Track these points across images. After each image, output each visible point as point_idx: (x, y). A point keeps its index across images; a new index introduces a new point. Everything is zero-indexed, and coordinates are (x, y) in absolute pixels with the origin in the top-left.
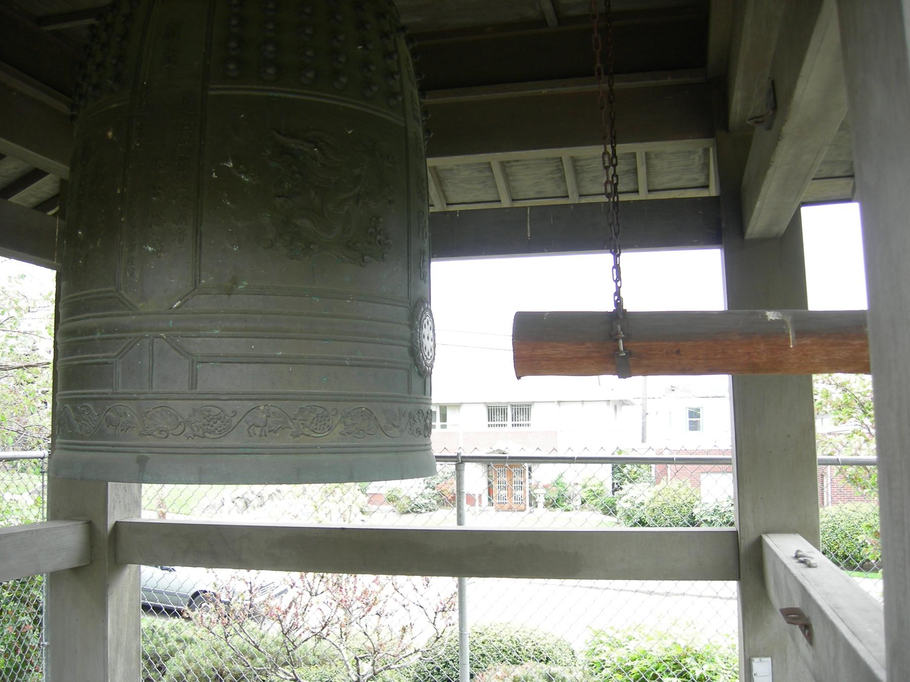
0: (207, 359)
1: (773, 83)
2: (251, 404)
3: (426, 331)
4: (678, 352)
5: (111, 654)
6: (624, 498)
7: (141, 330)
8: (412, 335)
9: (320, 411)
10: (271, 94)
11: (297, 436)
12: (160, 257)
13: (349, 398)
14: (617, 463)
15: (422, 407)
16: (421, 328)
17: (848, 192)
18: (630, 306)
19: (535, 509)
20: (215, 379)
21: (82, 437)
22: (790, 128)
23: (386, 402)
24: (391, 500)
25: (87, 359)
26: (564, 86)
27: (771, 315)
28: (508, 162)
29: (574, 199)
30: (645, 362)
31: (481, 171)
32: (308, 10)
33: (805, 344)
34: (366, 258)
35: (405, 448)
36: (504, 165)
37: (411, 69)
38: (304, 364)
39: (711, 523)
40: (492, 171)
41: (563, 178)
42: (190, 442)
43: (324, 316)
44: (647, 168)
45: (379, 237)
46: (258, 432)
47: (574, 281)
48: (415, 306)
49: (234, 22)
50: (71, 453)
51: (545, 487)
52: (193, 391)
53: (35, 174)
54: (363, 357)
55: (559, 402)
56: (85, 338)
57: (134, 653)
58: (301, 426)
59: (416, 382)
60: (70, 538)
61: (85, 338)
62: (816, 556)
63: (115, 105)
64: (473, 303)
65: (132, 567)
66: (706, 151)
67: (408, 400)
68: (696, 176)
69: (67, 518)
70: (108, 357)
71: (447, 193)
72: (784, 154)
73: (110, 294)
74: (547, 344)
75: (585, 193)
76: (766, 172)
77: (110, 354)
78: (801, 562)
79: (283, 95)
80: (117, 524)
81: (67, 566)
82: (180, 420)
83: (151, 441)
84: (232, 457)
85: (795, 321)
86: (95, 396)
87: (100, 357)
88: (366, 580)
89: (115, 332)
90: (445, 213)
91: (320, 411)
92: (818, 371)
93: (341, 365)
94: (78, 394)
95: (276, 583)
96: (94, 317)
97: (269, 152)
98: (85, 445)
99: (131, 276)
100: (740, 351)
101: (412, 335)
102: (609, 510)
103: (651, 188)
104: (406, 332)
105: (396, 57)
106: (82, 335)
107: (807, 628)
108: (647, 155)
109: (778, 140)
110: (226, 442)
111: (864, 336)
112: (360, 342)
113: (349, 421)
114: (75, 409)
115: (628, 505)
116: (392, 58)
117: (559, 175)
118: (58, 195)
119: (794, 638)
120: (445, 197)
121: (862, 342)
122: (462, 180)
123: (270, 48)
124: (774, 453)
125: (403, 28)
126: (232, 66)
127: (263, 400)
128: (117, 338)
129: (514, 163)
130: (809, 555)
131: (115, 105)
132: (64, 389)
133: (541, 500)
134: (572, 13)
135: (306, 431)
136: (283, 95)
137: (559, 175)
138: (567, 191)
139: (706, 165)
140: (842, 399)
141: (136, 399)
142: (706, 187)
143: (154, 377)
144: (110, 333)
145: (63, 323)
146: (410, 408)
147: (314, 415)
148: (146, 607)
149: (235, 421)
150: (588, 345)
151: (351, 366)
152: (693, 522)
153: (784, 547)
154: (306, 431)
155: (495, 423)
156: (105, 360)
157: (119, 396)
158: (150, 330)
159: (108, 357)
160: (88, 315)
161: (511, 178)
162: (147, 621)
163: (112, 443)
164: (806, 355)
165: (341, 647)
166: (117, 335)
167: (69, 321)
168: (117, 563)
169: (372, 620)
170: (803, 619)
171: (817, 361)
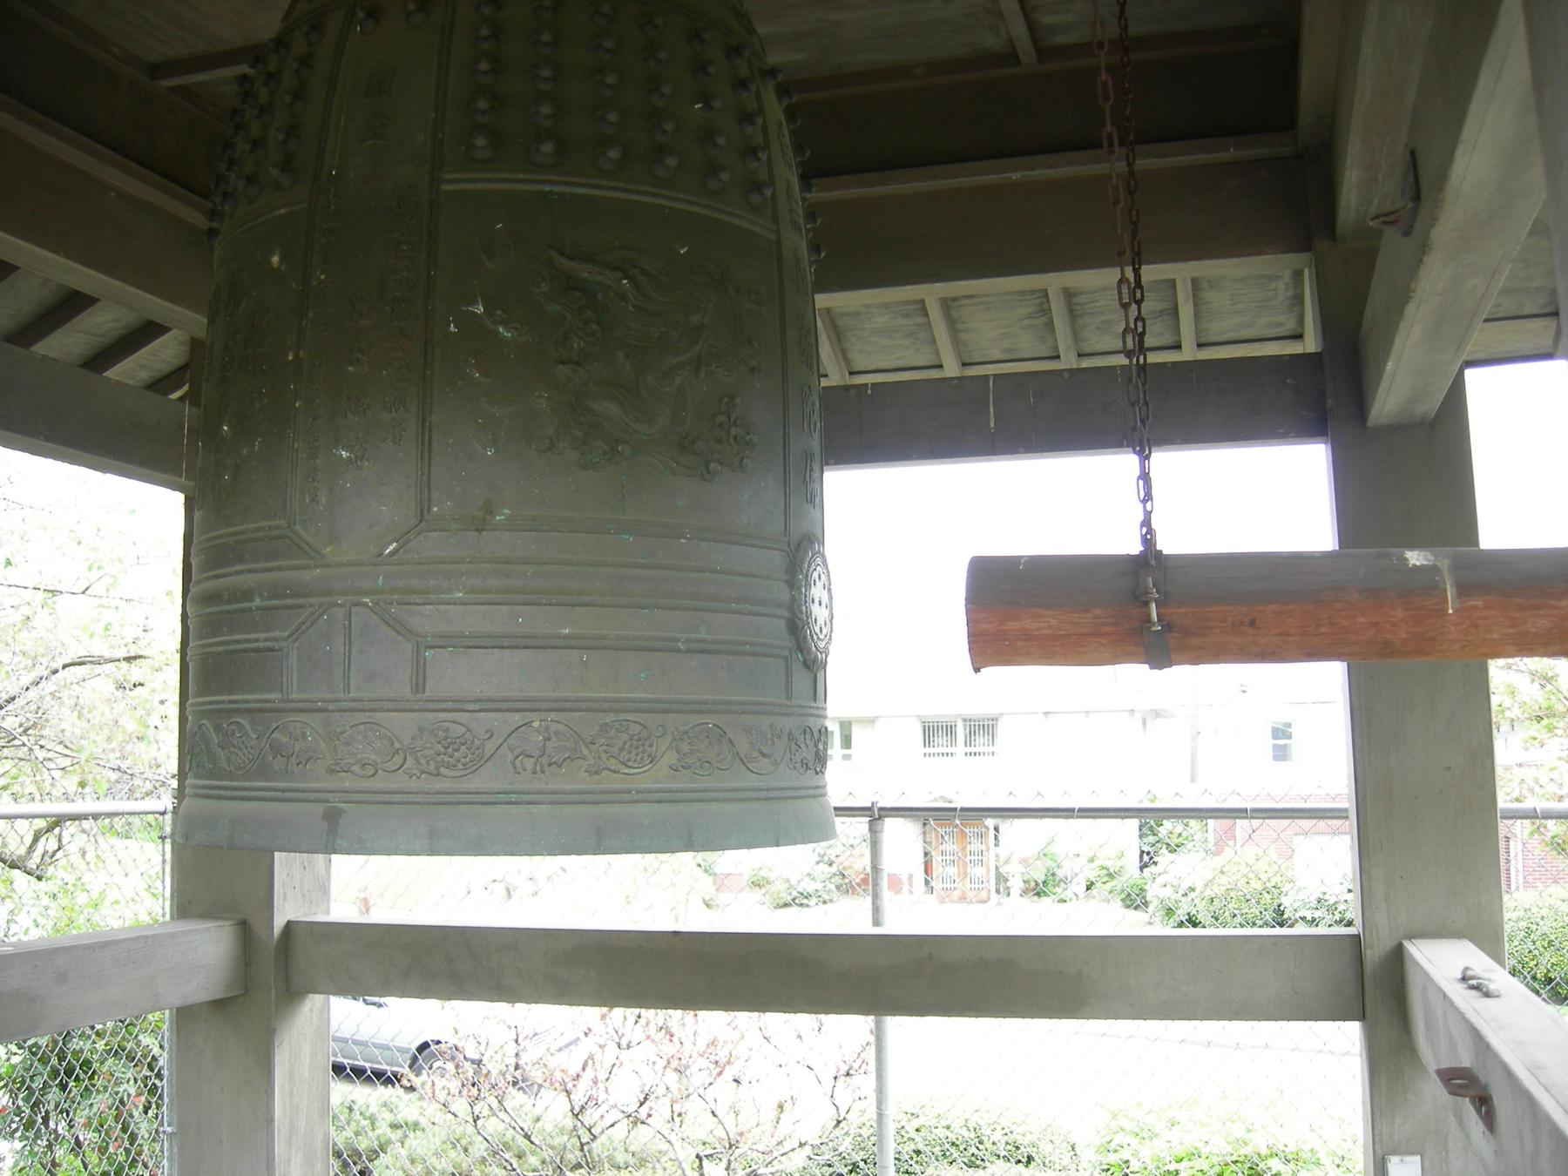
0: (445, 641)
1: (1413, 154)
2: (517, 719)
3: (817, 592)
4: (1252, 623)
5: (280, 1148)
6: (1160, 880)
7: (328, 593)
8: (793, 598)
9: (636, 729)
10: (547, 188)
11: (597, 773)
12: (361, 468)
14: (1149, 817)
15: (811, 721)
16: (808, 586)
17: (1546, 342)
18: (1169, 544)
19: (1007, 899)
20: (456, 675)
22: (1443, 232)
24: (756, 884)
25: (238, 642)
26: (1051, 166)
27: (1415, 558)
28: (955, 299)
29: (1068, 361)
30: (1196, 641)
31: (907, 316)
33: (1475, 608)
34: (712, 465)
36: (947, 304)
37: (787, 140)
38: (607, 648)
39: (1313, 922)
40: (927, 315)
41: (1050, 325)
42: (414, 784)
43: (641, 566)
44: (1196, 306)
45: (733, 431)
46: (530, 767)
47: (1073, 503)
51: (1024, 861)
52: (419, 696)
53: (148, 331)
54: (709, 637)
55: (1046, 713)
57: (319, 1146)
58: (604, 756)
59: (800, 678)
60: (209, 948)
62: (1498, 978)
63: (283, 211)
64: (899, 540)
65: (317, 999)
66: (1298, 274)
68: (1281, 318)
70: (274, 639)
72: (1434, 278)
73: (277, 532)
74: (1029, 610)
77: (277, 634)
78: (1473, 987)
79: (568, 190)
81: (205, 997)
82: (397, 745)
84: (485, 809)
85: (1456, 567)
86: (253, 705)
87: (260, 638)
88: (713, 1022)
89: (286, 596)
90: (847, 388)
91: (636, 729)
95: (556, 1030)
96: (249, 571)
97: (545, 287)
98: (235, 789)
99: (313, 500)
100: (1361, 620)
101: (793, 598)
102: (1135, 900)
103: (1204, 340)
105: (760, 121)
106: (229, 602)
107: (1484, 1103)
110: (477, 782)
114: (218, 729)
115: (1167, 893)
116: (753, 123)
117: (1044, 319)
118: (185, 367)
119: (1461, 1122)
122: (876, 330)
123: (546, 109)
124: (1423, 799)
125: (772, 72)
126: (480, 142)
129: (965, 301)
130: (1486, 975)
131: (283, 211)
132: (200, 694)
133: (1016, 884)
134: (1061, 40)
135: (613, 763)
136: (568, 190)
137: (1044, 319)
138: (1056, 348)
139: (1298, 299)
140: (1541, 700)
141: (321, 710)
142: (1298, 336)
143: (353, 673)
144: (277, 597)
145: (198, 582)
146: (789, 723)
147: (626, 737)
148: (338, 1069)
149: (490, 747)
150: (1097, 612)
151: (688, 651)
152: (1280, 919)
153: (1441, 962)
154: (613, 763)
155: (936, 750)
156: (269, 644)
158: (344, 592)
160: (238, 567)
161: (959, 326)
162: (341, 1092)
164: (1476, 626)
165: (673, 1137)
166: (289, 602)
167: (208, 579)
168: (291, 992)
169: (723, 1090)
170: (1477, 1087)
171: (1495, 636)
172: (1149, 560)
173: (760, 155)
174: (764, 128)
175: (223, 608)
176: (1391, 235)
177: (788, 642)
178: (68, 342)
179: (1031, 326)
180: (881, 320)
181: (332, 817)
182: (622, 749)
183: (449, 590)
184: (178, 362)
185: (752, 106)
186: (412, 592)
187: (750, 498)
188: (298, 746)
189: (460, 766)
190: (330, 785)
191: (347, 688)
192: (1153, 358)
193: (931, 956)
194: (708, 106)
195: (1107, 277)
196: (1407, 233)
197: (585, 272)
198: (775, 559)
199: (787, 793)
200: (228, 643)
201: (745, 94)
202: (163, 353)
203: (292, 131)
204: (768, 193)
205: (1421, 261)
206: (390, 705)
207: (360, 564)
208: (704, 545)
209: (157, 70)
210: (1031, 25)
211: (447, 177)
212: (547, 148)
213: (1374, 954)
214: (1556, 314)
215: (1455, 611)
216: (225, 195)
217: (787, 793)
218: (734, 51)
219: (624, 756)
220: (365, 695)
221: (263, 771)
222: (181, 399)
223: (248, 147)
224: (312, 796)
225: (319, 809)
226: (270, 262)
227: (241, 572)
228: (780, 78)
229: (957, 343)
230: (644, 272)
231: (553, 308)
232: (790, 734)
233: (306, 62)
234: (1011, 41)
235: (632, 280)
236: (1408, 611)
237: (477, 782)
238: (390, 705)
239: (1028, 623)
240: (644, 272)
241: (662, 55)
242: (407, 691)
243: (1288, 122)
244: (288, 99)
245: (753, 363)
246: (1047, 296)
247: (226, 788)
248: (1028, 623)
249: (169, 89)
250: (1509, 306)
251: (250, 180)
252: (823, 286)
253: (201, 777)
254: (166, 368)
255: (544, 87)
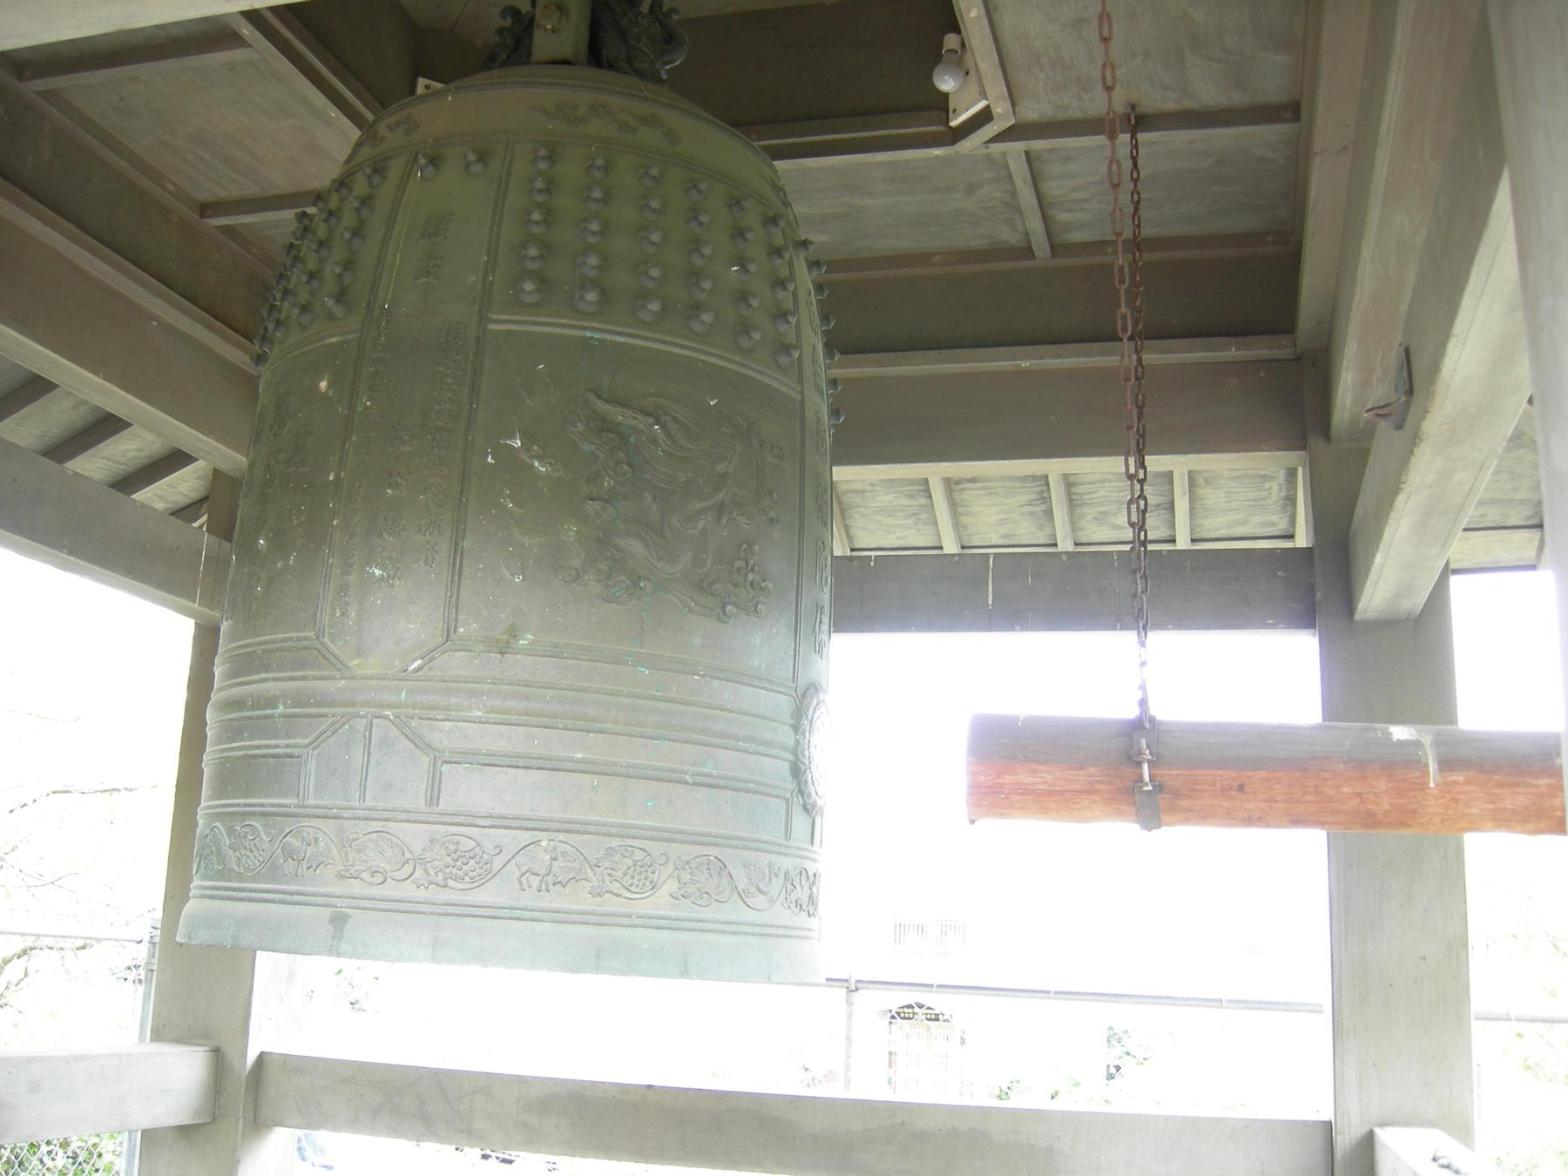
0: (462, 757)
1: (1407, 351)
2: (527, 837)
4: (1241, 788)
7: (352, 704)
8: (797, 742)
9: (640, 855)
12: (392, 586)
13: (688, 838)
15: (807, 864)
17: (1529, 554)
18: (1162, 711)
20: (470, 790)
21: (240, 877)
22: (1433, 425)
23: (748, 849)
25: (258, 747)
26: (1059, 356)
28: (958, 482)
30: (1185, 803)
31: (910, 496)
32: (655, 204)
33: (1455, 783)
34: (729, 607)
35: (774, 931)
36: (950, 485)
37: (814, 308)
38: (614, 774)
40: (930, 497)
41: (1049, 513)
42: (421, 894)
43: (657, 699)
44: (1191, 501)
45: (751, 577)
46: (535, 884)
48: (804, 695)
49: (536, 216)
50: (216, 903)
52: (433, 809)
53: (175, 460)
54: (715, 773)
56: (258, 713)
58: (607, 879)
59: (800, 822)
61: (258, 713)
63: (334, 340)
64: (895, 706)
66: (1291, 474)
67: (783, 850)
68: (1274, 518)
69: (179, 1040)
70: (295, 746)
71: (852, 531)
72: (1424, 470)
73: (305, 643)
75: (1084, 540)
76: (1392, 502)
77: (298, 740)
78: (1443, 1166)
79: (609, 337)
80: (262, 1057)
82: (408, 855)
83: (356, 888)
84: (490, 922)
85: (1438, 743)
87: (280, 744)
89: (312, 705)
90: (850, 559)
91: (640, 855)
92: (1473, 828)
93: (679, 782)
94: (238, 805)
96: (275, 679)
97: (580, 427)
98: (243, 890)
99: (343, 614)
100: (1345, 789)
101: (797, 742)
103: (1197, 536)
104: (790, 740)
105: (791, 287)
108: (1192, 478)
109: (1414, 445)
110: (484, 896)
111: (1557, 773)
112: (712, 746)
113: (686, 876)
114: (231, 831)
116: (785, 289)
117: (1043, 507)
118: (205, 499)
120: (849, 537)
121: (1552, 781)
122: (883, 505)
123: (593, 260)
125: (805, 244)
126: (529, 286)
127: (547, 830)
128: (313, 716)
129: (969, 485)
131: (334, 340)
132: (214, 797)
134: (1075, 237)
136: (609, 337)
137: (1043, 507)
139: (1291, 500)
141: (336, 817)
143: (369, 783)
145: (220, 690)
146: (786, 863)
147: (630, 862)
149: (498, 863)
150: (1092, 770)
156: (289, 750)
157: (308, 811)
158: (367, 704)
159: (295, 746)
160: (264, 675)
161: (961, 510)
163: (291, 888)
164: (1456, 801)
166: (313, 710)
167: (231, 686)
168: (258, 1124)
171: (1475, 811)
172: (1142, 726)
173: (790, 319)
174: (795, 295)
175: (245, 714)
176: (1384, 426)
177: (791, 784)
178: (96, 464)
179: (1031, 513)
180: (885, 499)
181: (339, 921)
182: (625, 874)
183: (470, 709)
184: (195, 496)
185: (784, 272)
186: (434, 708)
187: (762, 642)
188: (310, 850)
189: (467, 879)
190: (338, 890)
191: (363, 797)
192: (1150, 547)
193: (903, 1123)
194: (743, 266)
195: (1114, 465)
196: (1399, 427)
197: (619, 415)
198: (784, 703)
199: (781, 931)
200: (247, 748)
201: (779, 261)
202: (182, 485)
203: (349, 265)
204: (796, 355)
205: (1412, 452)
206: (404, 816)
207: (385, 678)
208: (716, 683)
209: (206, 209)
210: (1046, 219)
211: (495, 317)
212: (592, 296)
213: (1345, 1141)
214: (1540, 526)
215: (1437, 785)
216: (278, 323)
217: (781, 931)
218: (773, 220)
219: (627, 880)
220: (380, 805)
221: (273, 873)
222: (201, 527)
223: (305, 278)
224: (319, 900)
225: (327, 912)
226: (317, 386)
227: (267, 680)
228: (812, 248)
229: (957, 526)
230: (675, 420)
231: (588, 448)
232: (787, 873)
233: (366, 201)
234: (1027, 234)
235: (663, 426)
236: (1392, 790)
237: (484, 896)
238: (404, 816)
239: (1024, 778)
240: (675, 420)
241: (704, 219)
242: (421, 803)
243: (1291, 330)
244: (347, 235)
245: (773, 514)
246: (1047, 484)
247: (234, 889)
248: (1024, 778)
249: (219, 228)
250: (1493, 515)
251: (304, 309)
252: (839, 460)
253: (210, 879)
254: (182, 501)
255: (592, 240)
